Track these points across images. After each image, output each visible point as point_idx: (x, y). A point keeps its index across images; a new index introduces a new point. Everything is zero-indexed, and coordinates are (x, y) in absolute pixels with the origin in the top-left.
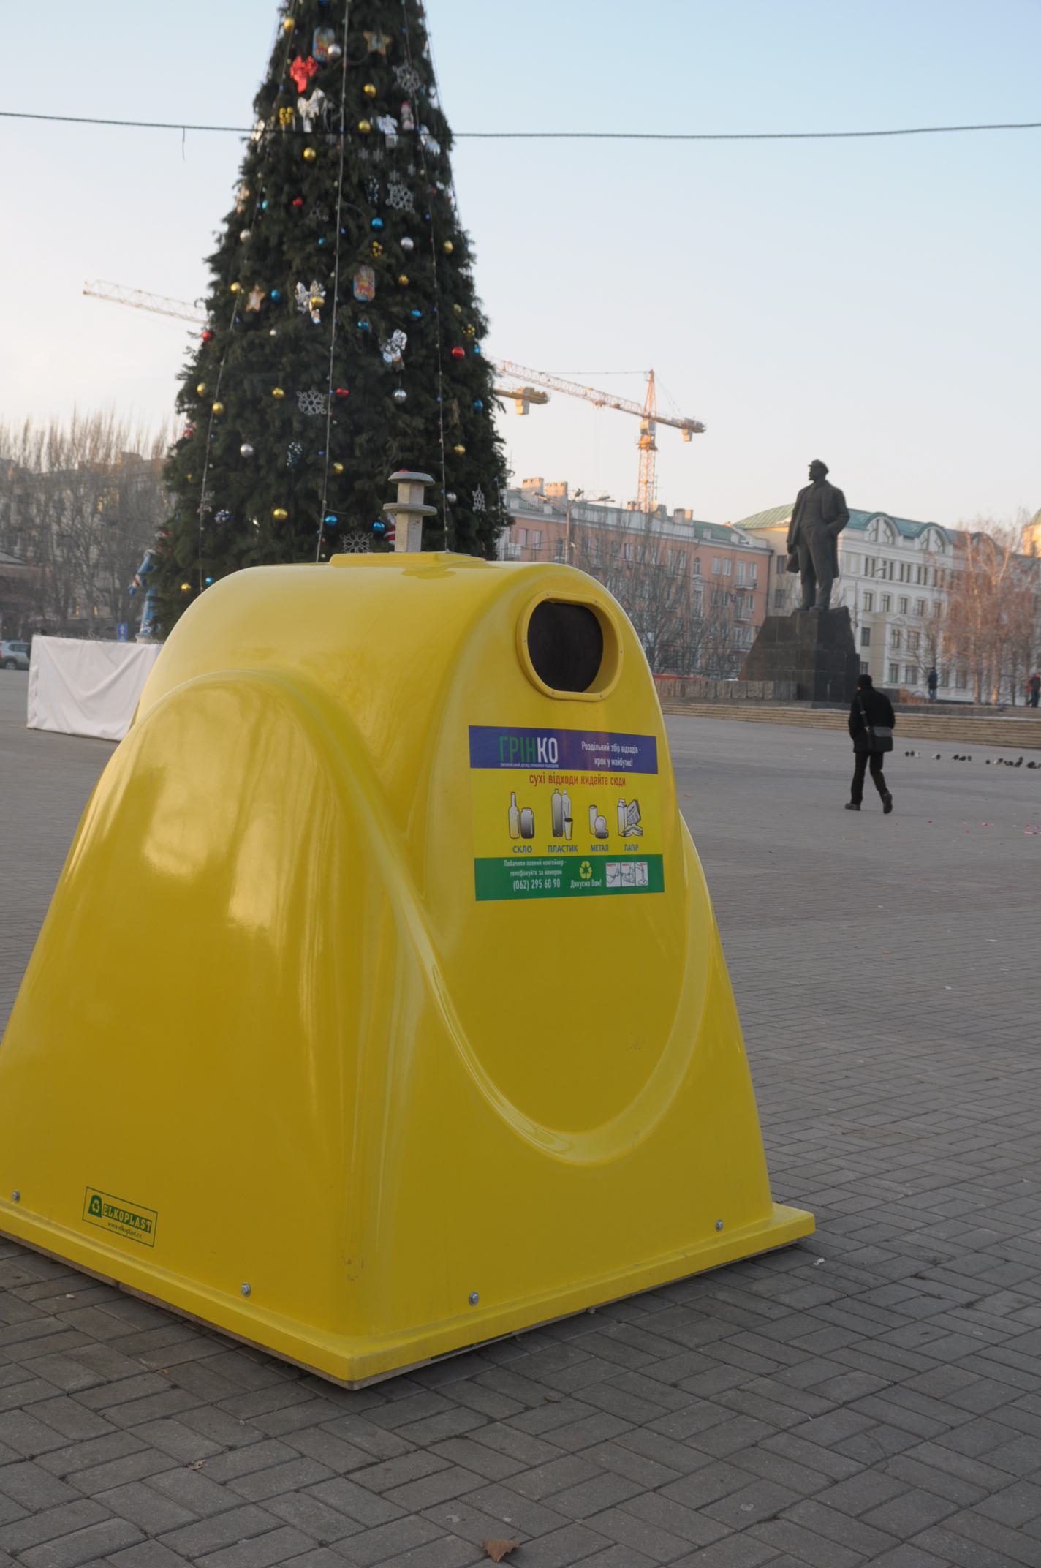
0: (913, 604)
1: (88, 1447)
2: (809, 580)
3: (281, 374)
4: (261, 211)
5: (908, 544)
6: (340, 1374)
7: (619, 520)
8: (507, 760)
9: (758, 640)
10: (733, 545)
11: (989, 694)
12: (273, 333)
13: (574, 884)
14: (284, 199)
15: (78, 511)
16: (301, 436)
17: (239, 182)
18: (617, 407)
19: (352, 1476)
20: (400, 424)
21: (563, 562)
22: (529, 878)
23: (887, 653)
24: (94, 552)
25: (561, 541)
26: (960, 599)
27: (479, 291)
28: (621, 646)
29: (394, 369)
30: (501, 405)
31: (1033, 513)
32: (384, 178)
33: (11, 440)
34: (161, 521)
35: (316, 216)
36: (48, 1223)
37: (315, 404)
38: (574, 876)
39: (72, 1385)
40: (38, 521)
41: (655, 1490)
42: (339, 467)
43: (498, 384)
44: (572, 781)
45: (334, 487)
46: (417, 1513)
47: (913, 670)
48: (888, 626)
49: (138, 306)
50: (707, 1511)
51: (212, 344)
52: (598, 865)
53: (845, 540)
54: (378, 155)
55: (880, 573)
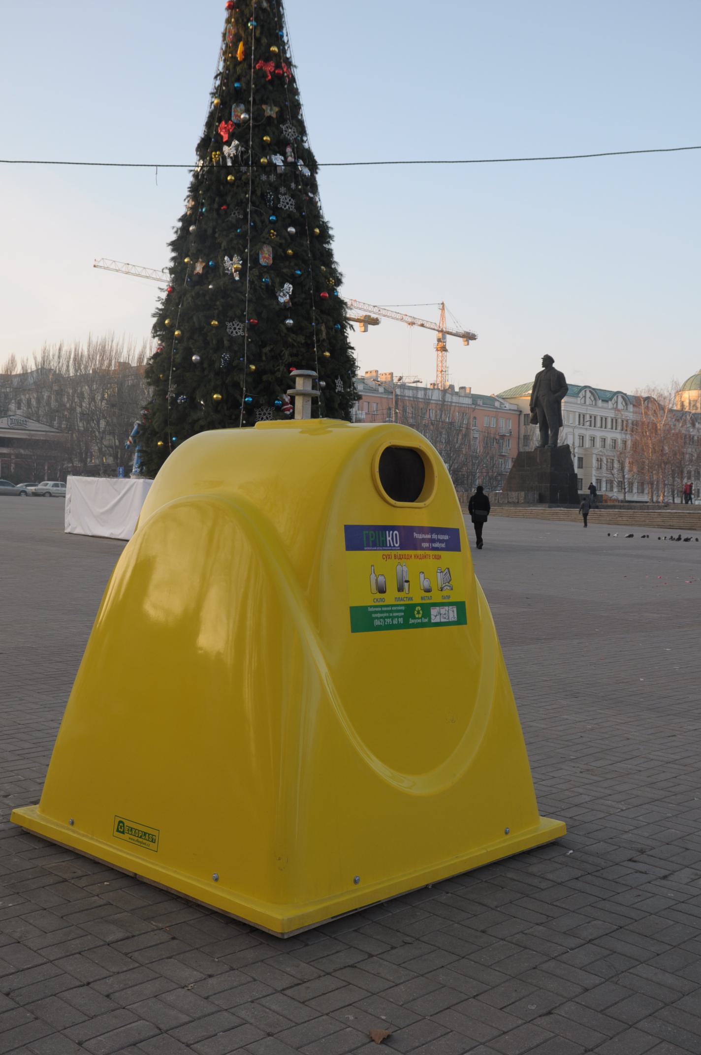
0: (609, 442)
2: (544, 429)
3: (216, 312)
4: (202, 214)
5: (605, 405)
6: (276, 929)
7: (425, 395)
8: (368, 546)
9: (514, 466)
10: (497, 408)
11: (658, 496)
12: (210, 287)
13: (411, 621)
14: (216, 206)
15: (93, 399)
17: (188, 197)
18: (422, 325)
19: (287, 992)
20: (290, 340)
21: (392, 422)
22: (384, 618)
23: (594, 472)
24: (103, 423)
25: (390, 409)
26: (638, 438)
27: (336, 258)
28: (436, 474)
29: (285, 306)
30: (351, 326)
32: (276, 191)
33: (51, 357)
34: (144, 403)
35: (235, 215)
36: (92, 839)
37: (237, 330)
38: (412, 616)
39: (110, 938)
40: (68, 405)
41: (474, 997)
42: (253, 367)
43: (350, 314)
44: (409, 557)
46: (327, 1014)
47: (610, 482)
48: (594, 456)
49: (127, 273)
50: (508, 1009)
52: (426, 608)
53: (566, 404)
54: (273, 178)
55: (588, 423)
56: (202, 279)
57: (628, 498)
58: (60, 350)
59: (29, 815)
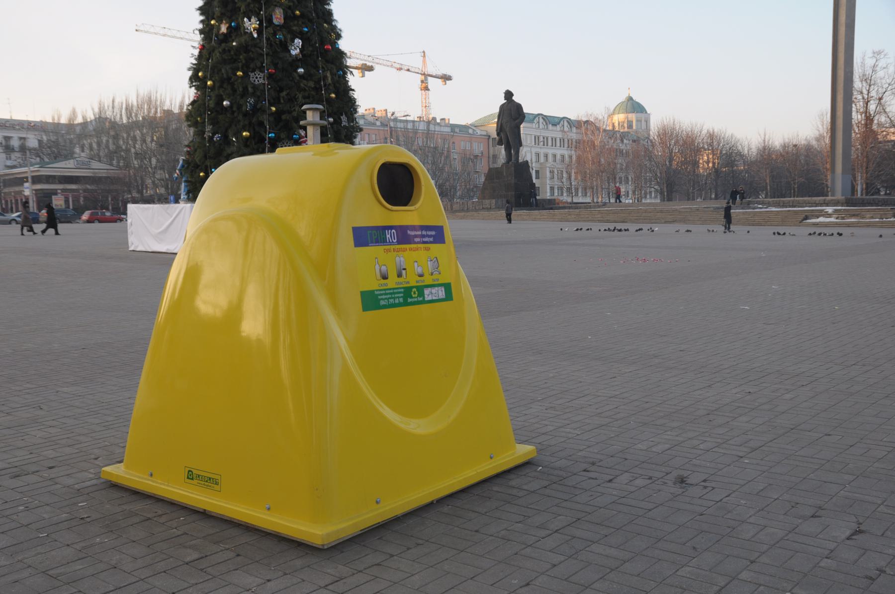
0: (558, 157)
1: (200, 586)
2: (508, 149)
3: (240, 64)
5: (554, 128)
6: (318, 542)
13: (410, 300)
15: (144, 141)
16: (253, 94)
18: (408, 70)
20: (302, 85)
23: (548, 182)
24: (154, 161)
27: (336, 16)
30: (351, 72)
31: (612, 110)
34: (186, 143)
37: (258, 78)
38: (410, 296)
39: (188, 559)
40: (124, 147)
42: (274, 109)
43: (349, 62)
44: (405, 250)
45: (272, 119)
47: (561, 189)
49: (164, 35)
51: (205, 51)
52: (420, 290)
56: (226, 38)
57: (575, 200)
58: (113, 101)
59: (116, 472)
